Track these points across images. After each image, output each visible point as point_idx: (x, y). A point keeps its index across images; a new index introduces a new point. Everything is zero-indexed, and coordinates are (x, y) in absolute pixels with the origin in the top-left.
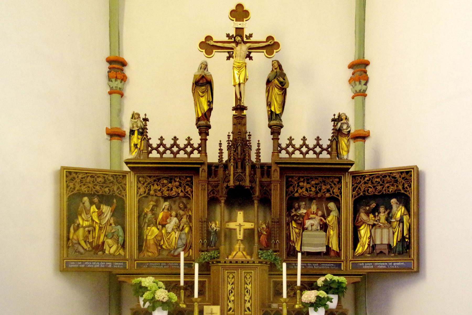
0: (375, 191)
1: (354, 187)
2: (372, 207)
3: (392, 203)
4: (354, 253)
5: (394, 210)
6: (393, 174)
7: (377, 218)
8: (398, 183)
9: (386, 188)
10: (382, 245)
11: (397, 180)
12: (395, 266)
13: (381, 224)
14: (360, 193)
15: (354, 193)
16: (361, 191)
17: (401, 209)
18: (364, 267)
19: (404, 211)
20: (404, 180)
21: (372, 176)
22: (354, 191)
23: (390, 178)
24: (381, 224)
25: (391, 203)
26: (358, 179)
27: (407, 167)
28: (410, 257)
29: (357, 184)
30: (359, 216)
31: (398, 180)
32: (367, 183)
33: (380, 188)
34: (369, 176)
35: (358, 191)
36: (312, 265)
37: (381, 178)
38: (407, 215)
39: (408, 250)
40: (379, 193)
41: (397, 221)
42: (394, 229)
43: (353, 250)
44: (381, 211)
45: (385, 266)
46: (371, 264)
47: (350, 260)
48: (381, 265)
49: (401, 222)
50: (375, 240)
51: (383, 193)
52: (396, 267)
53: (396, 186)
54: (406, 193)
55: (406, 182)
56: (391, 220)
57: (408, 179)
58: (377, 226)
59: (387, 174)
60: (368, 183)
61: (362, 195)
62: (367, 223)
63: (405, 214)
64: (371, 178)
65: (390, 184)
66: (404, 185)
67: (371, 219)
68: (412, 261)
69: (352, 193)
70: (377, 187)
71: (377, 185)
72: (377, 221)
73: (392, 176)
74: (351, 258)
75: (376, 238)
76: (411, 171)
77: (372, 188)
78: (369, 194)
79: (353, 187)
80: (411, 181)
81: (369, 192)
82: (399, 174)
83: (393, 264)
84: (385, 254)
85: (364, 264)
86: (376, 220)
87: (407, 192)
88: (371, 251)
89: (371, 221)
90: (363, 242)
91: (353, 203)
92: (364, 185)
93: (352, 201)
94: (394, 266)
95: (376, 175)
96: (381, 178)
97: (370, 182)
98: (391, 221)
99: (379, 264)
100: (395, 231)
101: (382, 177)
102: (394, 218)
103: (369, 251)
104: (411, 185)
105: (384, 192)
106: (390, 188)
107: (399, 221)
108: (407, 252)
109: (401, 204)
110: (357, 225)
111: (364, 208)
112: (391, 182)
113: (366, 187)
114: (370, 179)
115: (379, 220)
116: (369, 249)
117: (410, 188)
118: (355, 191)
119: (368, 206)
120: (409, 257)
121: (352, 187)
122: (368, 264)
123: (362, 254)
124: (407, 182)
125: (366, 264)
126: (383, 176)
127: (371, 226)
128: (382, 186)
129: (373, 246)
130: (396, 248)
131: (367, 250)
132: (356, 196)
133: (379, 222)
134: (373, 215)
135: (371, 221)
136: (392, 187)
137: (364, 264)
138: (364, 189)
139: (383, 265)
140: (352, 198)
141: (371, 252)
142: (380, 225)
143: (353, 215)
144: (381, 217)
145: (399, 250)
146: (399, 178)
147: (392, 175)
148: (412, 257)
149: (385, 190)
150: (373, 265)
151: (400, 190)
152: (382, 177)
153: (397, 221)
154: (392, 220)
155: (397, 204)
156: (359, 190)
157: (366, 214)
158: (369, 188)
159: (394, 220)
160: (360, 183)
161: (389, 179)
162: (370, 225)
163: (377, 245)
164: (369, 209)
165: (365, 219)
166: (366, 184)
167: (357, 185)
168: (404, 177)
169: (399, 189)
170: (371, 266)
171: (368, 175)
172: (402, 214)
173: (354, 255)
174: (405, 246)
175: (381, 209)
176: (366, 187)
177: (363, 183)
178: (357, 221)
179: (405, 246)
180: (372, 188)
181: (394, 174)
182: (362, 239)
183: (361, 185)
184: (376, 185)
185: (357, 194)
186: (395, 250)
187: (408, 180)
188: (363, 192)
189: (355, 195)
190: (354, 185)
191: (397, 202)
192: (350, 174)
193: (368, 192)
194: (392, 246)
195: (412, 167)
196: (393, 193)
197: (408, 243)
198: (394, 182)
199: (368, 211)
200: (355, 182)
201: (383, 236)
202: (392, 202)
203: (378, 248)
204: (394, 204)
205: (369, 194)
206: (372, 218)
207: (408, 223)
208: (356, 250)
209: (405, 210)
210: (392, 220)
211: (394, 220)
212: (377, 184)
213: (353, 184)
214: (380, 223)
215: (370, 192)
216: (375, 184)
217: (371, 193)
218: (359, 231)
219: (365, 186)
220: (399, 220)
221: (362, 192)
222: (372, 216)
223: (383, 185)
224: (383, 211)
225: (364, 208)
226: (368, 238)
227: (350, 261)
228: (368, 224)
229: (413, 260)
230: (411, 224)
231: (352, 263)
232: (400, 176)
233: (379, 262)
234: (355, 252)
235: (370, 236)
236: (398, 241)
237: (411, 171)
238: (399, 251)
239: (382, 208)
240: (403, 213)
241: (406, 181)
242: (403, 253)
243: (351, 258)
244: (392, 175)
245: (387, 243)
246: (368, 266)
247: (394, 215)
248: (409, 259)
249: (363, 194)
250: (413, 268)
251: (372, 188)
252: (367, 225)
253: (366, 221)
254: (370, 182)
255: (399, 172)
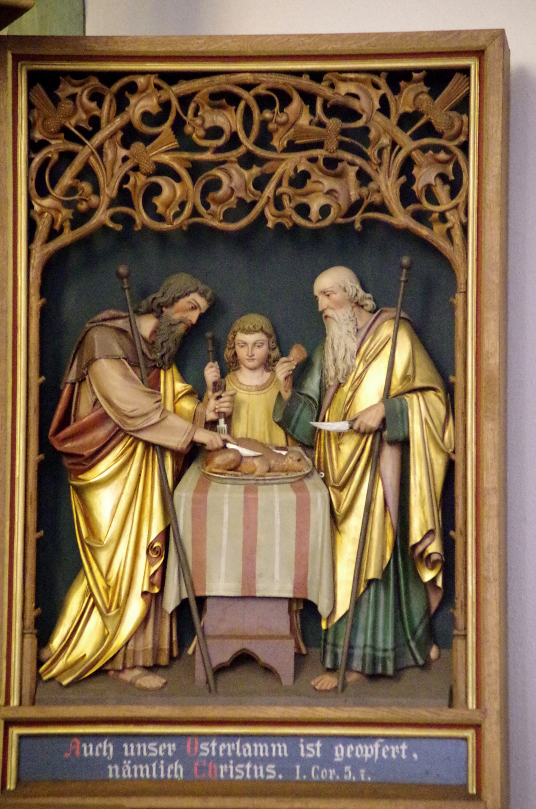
0: (207, 206)
1: (46, 161)
2: (177, 317)
3: (323, 302)
4: (40, 663)
5: (341, 354)
6: (332, 86)
7: (212, 403)
8: (372, 152)
9: (285, 188)
10: (252, 603)
11: (366, 130)
12: (347, 768)
13: (245, 452)
14: (92, 211)
15: (47, 202)
16: (97, 191)
17: (388, 350)
18: (113, 772)
19: (412, 360)
20: (415, 137)
21: (184, 87)
22: (43, 193)
23: (313, 111)
24: (245, 452)
25: (315, 300)
26: (73, 97)
27: (404, 36)
28: (451, 705)
29: (70, 136)
30: (82, 379)
31: (372, 135)
32: (148, 139)
33: (237, 181)
34: (158, 87)
35: (72, 190)
36: (294, 750)
37: (248, 111)
38: (431, 395)
39: (434, 652)
40: (229, 216)
41: (363, 434)
42: (341, 488)
43: (31, 642)
44: (242, 353)
45: (271, 768)
46: (171, 747)
47: (10, 714)
48: (244, 760)
49: (392, 443)
50: (201, 564)
51: (262, 218)
52: (349, 776)
53: (352, 172)
54: (424, 231)
55: (424, 149)
56: (319, 425)
57: (439, 127)
58: (219, 460)
59: (293, 81)
60: (155, 136)
61: (104, 228)
62: (139, 435)
63: (418, 384)
64: (175, 103)
65: (313, 160)
66: (415, 171)
67: (169, 406)
68: (470, 734)
69: (30, 206)
70: (218, 173)
71: (221, 156)
72: (212, 425)
73: (325, 102)
74: (15, 701)
75: (210, 558)
76: (466, 71)
77: (177, 178)
78: (161, 218)
79: (38, 159)
80: (465, 147)
81: (160, 209)
82: (377, 87)
83: (328, 752)
84: (268, 670)
85: (119, 750)
86: (211, 416)
87: (430, 226)
88: (166, 645)
89: (172, 420)
90: (113, 575)
91: (36, 282)
92: (122, 152)
93: (36, 261)
94: (341, 772)
95: (217, 79)
96: (248, 111)
97: (166, 128)
98: (315, 431)
99: (230, 746)
100: (345, 506)
101: (258, 98)
102: (337, 407)
103: (157, 650)
104: (458, 171)
105: (270, 213)
106: (310, 185)
107: (378, 432)
108: (427, 665)
109: (392, 312)
110: (68, 446)
111: (120, 323)
112: (320, 145)
113: (136, 169)
114: (166, 106)
115: (229, 419)
116: (157, 634)
117: (453, 194)
118: (57, 192)
119: (149, 311)
120: (446, 701)
121: (30, 161)
122: (142, 748)
123: (102, 671)
124: (437, 149)
125: (128, 749)
126: (261, 90)
127: (169, 462)
128: (256, 170)
129: (183, 606)
130: (354, 628)
131: (140, 643)
132: (61, 230)
133: (229, 432)
134: (185, 379)
135: (172, 420)
136: (328, 183)
137: (119, 750)
138: (126, 179)
139: (255, 760)
140: (31, 239)
141: (164, 660)
142: (242, 457)
143: (42, 372)
144: (242, 395)
145: (374, 648)
146: (380, 118)
147: (322, 89)
148: (472, 703)
149: (278, 203)
150: (179, 755)
151: (383, 208)
152: (258, 98)
153: (363, 434)
154: (324, 426)
155: (359, 305)
156: (86, 187)
157: (135, 365)
158: (160, 180)
159: (344, 426)
160: (89, 135)
161: (304, 120)
162: (162, 449)
163: (209, 602)
164: (154, 332)
165: (127, 408)
166: (138, 146)
167: (72, 146)
168: (415, 116)
169: (376, 198)
170: (169, 760)
171: (153, 80)
172: (396, 386)
173: (39, 677)
174: (417, 619)
175: (241, 337)
176: (136, 169)
177: (112, 136)
178: (65, 422)
179: (417, 619)
180: (184, 174)
181: (343, 88)
182: (104, 557)
183: (100, 150)
184: (208, 156)
185: (66, 213)
186: (343, 642)
187: (439, 135)
188: (112, 204)
189: (53, 221)
190: (43, 144)
191: (361, 293)
192: (16, 59)
193: (150, 208)
194: (318, 617)
195: (474, 45)
196: (334, 226)
197: (435, 601)
198: (342, 146)
199: (151, 344)
200: (53, 124)
201: (261, 537)
202: (325, 293)
203: (223, 628)
204: (339, 305)
205: (161, 218)
206: (176, 399)
207: (441, 450)
208: (56, 642)
209: (417, 353)
210: (324, 426)
211: (344, 426)
212: (218, 150)
213: (38, 136)
214: (240, 442)
215: (168, 206)
216: (204, 149)
217: (177, 215)
218: (81, 491)
219: (125, 159)
220: (373, 422)
221: (105, 201)
222: (180, 386)
223: (261, 161)
224: (260, 353)
225: (120, 323)
226: (150, 548)
227: (9, 723)
228: (148, 445)
229: (477, 727)
230: (458, 459)
231: (21, 737)
232: (384, 101)
233: (233, 737)
234: (45, 654)
235: (165, 535)
236: (370, 582)
237: (466, 71)
238: (374, 660)
239: (249, 332)
240: (405, 378)
241: (426, 141)
242: (399, 671)
243: (15, 701)
244: (322, 89)
245: (290, 594)
246: (148, 761)
247: (339, 385)
248: (448, 715)
249: (113, 218)
250: (472, 790)
251: (177, 178)
252: (140, 448)
253: (140, 423)
254: (166, 128)
255: (377, 72)
